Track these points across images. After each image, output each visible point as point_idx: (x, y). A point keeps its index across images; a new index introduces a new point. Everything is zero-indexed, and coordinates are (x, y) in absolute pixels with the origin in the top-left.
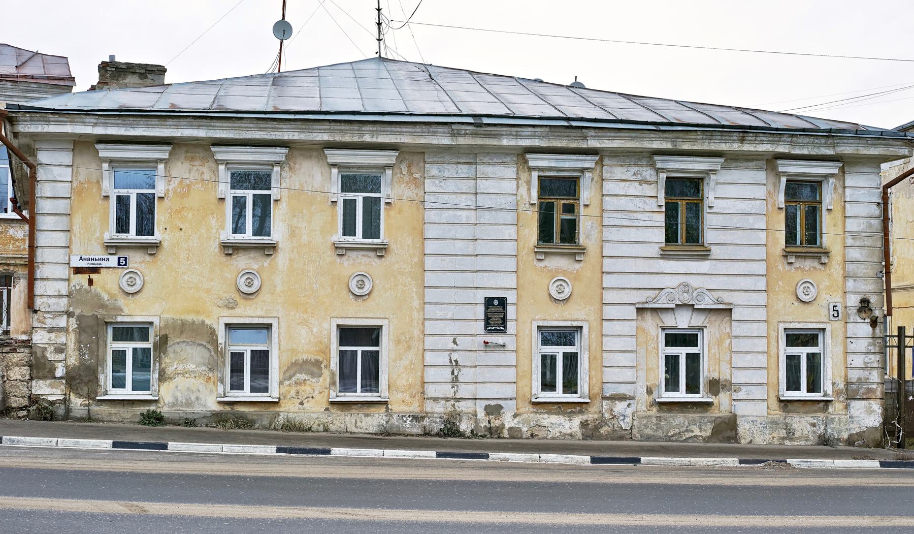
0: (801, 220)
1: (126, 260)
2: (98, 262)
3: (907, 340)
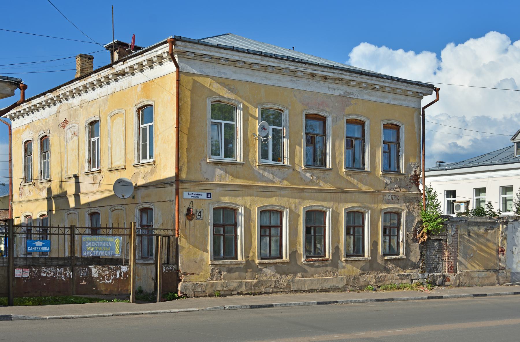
0: (210, 232)
1: (210, 195)
2: (197, 196)
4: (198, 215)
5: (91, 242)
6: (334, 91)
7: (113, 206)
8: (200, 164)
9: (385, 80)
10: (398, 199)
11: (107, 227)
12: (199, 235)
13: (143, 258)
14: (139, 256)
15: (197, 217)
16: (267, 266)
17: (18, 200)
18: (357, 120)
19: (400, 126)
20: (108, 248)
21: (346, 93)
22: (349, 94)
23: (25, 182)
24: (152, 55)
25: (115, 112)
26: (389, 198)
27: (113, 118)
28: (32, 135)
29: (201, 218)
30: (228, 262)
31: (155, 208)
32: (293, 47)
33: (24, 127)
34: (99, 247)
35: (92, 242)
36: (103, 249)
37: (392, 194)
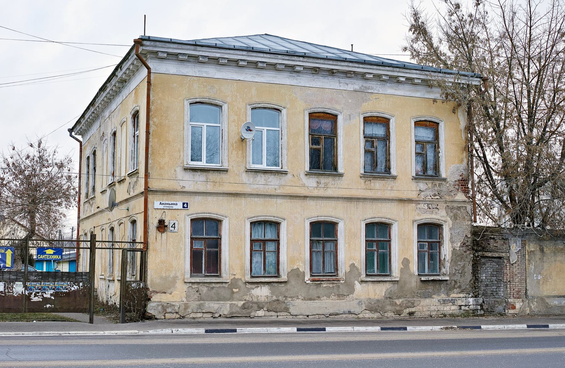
2: (171, 206)
3: (97, 244)
4: (172, 227)
8: (175, 171)
9: (411, 70)
15: (171, 229)
16: (259, 286)
21: (363, 88)
29: (175, 231)
37: (428, 203)
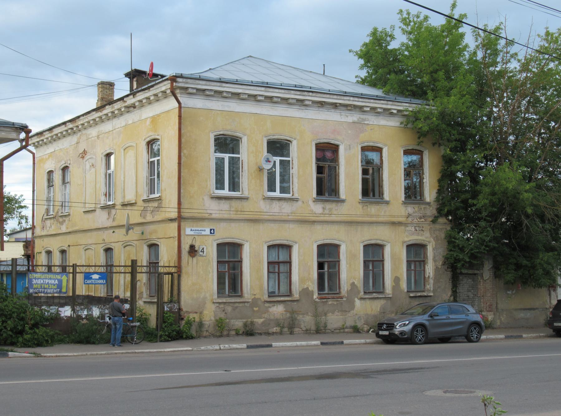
1: (214, 231)
4: (201, 252)
5: (38, 279)
6: (346, 118)
7: (125, 242)
8: (203, 199)
10: (422, 230)
11: (120, 265)
12: (202, 272)
13: (151, 296)
14: (147, 294)
17: (40, 235)
18: (374, 147)
19: (423, 152)
20: (55, 286)
21: (360, 120)
22: (365, 120)
23: (47, 215)
24: (158, 91)
25: (127, 145)
26: (412, 230)
27: (126, 150)
28: (54, 165)
30: (233, 300)
31: (161, 244)
32: (324, 65)
33: (47, 157)
34: (45, 285)
35: (39, 279)
36: (49, 286)
